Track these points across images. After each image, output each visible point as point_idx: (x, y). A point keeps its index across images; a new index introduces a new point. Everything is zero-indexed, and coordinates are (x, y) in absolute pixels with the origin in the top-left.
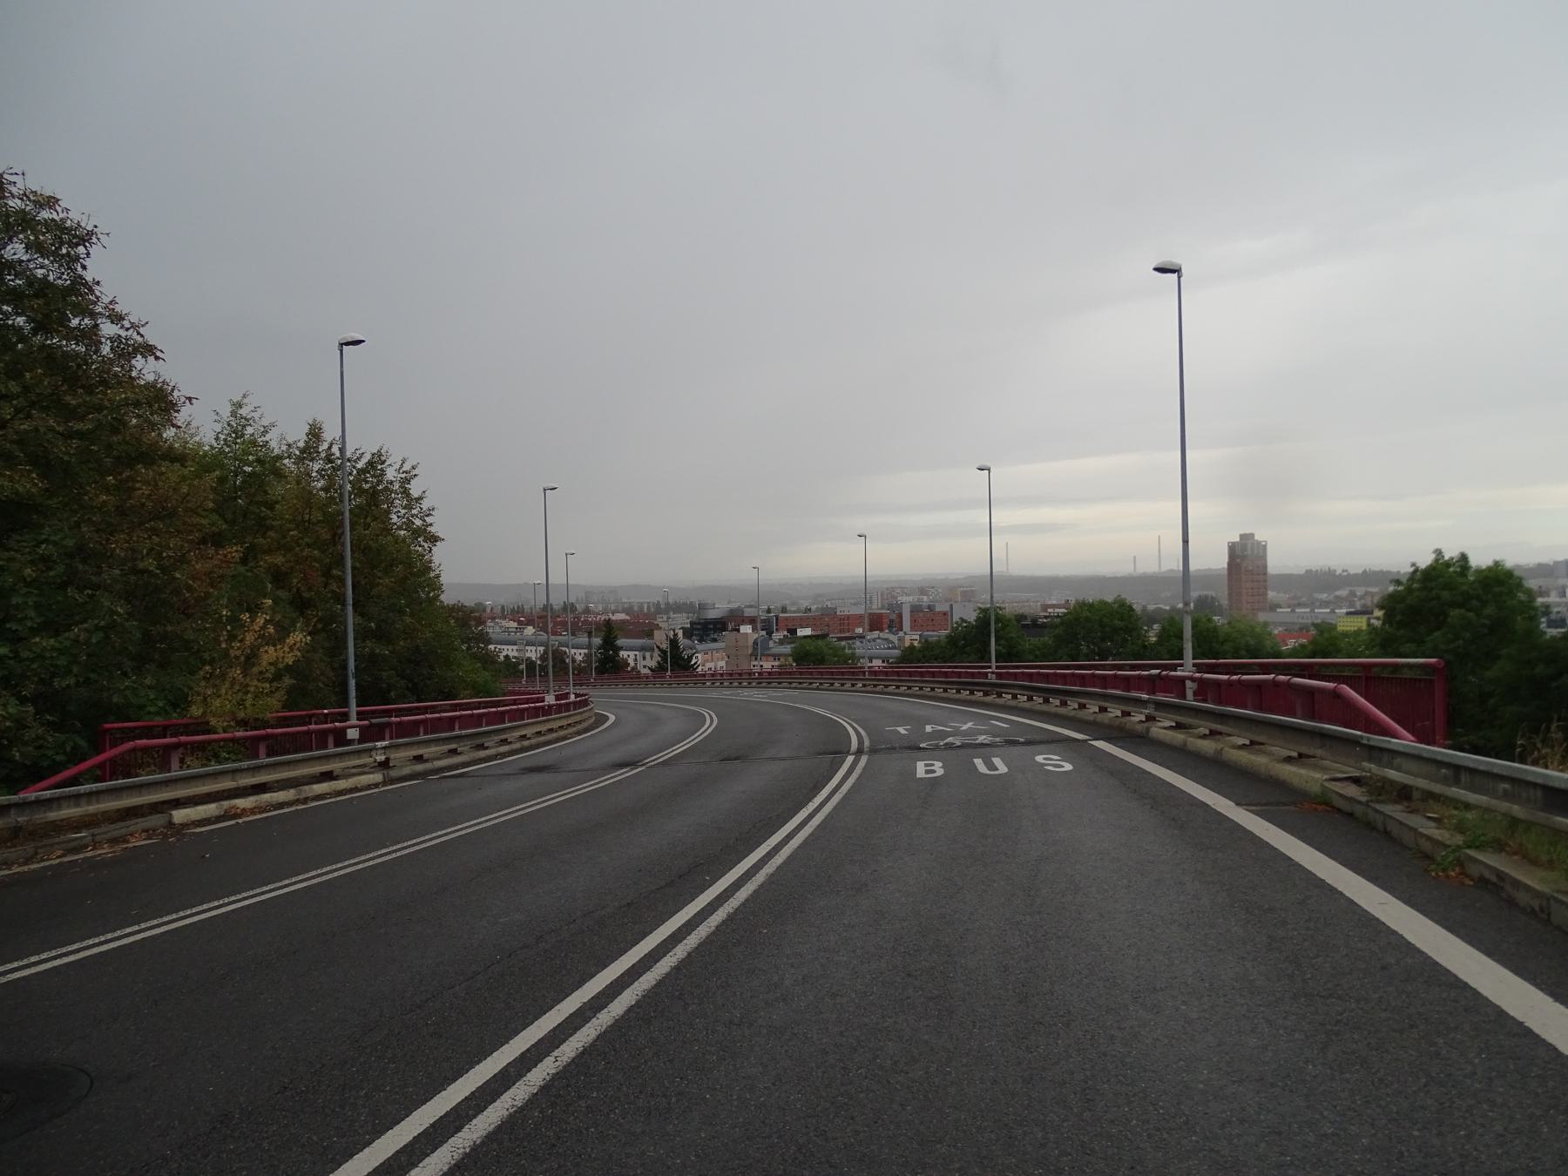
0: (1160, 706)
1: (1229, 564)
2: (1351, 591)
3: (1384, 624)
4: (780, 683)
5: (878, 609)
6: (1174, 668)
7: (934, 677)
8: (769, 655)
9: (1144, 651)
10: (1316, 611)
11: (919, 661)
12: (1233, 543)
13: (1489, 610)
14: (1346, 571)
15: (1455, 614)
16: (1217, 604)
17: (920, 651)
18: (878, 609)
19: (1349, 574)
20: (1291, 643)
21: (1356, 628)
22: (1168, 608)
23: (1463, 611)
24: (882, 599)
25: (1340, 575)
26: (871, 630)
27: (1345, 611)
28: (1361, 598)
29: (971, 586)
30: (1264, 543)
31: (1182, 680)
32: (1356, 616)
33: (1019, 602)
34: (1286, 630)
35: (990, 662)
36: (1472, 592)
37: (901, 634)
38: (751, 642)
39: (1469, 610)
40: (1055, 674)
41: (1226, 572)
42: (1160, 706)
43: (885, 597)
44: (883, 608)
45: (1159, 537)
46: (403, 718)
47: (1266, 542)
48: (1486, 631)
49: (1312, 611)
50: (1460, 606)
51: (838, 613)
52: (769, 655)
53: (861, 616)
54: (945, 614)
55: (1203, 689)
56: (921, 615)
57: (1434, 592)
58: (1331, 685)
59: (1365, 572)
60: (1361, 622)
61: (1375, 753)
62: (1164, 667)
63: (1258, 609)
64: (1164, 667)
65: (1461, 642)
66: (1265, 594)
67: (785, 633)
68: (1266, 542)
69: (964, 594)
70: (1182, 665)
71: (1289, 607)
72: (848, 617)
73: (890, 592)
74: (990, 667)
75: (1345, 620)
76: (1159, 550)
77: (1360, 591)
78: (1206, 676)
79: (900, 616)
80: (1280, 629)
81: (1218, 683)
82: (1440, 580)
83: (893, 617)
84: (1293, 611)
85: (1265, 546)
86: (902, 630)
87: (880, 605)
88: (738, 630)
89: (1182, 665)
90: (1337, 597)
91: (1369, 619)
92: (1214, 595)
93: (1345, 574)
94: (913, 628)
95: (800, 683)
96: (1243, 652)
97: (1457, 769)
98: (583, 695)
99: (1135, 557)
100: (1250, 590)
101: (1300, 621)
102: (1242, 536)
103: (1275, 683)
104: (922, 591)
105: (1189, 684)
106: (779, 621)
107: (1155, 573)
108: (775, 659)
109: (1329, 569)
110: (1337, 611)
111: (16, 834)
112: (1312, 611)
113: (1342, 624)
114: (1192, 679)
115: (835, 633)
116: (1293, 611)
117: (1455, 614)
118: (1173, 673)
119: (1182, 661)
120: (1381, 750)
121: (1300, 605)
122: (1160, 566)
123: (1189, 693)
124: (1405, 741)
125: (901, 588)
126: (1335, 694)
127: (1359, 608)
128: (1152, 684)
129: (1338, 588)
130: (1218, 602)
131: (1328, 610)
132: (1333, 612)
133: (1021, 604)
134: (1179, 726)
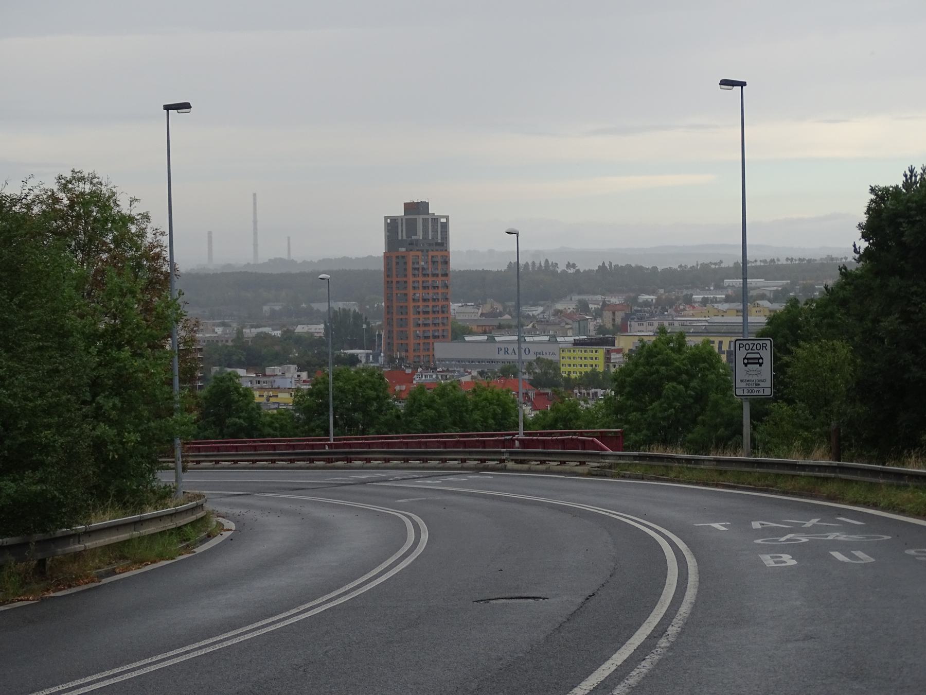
1: (387, 257)
2: (580, 301)
7: (275, 450)
13: (694, 383)
14: (574, 266)
19: (578, 271)
21: (589, 369)
22: (278, 333)
23: (675, 384)
27: (571, 339)
28: (598, 314)
30: (443, 220)
32: (588, 348)
39: (680, 383)
41: (381, 267)
45: (255, 195)
46: (506, 437)
47: (447, 218)
48: (691, 400)
58: (591, 438)
59: (602, 268)
60: (597, 358)
63: (435, 337)
66: (445, 310)
68: (447, 218)
70: (518, 434)
71: (484, 333)
75: (572, 354)
76: (255, 222)
77: (594, 301)
82: (659, 357)
84: (491, 340)
85: (445, 226)
90: (558, 312)
91: (608, 352)
93: (571, 271)
99: (210, 233)
100: (421, 304)
101: (502, 356)
109: (547, 261)
110: (559, 339)
113: (566, 361)
117: (668, 385)
120: (607, 455)
124: (610, 452)
126: (592, 441)
127: (593, 333)
128: (503, 444)
129: (560, 298)
130: (368, 324)
131: (547, 338)
132: (553, 340)
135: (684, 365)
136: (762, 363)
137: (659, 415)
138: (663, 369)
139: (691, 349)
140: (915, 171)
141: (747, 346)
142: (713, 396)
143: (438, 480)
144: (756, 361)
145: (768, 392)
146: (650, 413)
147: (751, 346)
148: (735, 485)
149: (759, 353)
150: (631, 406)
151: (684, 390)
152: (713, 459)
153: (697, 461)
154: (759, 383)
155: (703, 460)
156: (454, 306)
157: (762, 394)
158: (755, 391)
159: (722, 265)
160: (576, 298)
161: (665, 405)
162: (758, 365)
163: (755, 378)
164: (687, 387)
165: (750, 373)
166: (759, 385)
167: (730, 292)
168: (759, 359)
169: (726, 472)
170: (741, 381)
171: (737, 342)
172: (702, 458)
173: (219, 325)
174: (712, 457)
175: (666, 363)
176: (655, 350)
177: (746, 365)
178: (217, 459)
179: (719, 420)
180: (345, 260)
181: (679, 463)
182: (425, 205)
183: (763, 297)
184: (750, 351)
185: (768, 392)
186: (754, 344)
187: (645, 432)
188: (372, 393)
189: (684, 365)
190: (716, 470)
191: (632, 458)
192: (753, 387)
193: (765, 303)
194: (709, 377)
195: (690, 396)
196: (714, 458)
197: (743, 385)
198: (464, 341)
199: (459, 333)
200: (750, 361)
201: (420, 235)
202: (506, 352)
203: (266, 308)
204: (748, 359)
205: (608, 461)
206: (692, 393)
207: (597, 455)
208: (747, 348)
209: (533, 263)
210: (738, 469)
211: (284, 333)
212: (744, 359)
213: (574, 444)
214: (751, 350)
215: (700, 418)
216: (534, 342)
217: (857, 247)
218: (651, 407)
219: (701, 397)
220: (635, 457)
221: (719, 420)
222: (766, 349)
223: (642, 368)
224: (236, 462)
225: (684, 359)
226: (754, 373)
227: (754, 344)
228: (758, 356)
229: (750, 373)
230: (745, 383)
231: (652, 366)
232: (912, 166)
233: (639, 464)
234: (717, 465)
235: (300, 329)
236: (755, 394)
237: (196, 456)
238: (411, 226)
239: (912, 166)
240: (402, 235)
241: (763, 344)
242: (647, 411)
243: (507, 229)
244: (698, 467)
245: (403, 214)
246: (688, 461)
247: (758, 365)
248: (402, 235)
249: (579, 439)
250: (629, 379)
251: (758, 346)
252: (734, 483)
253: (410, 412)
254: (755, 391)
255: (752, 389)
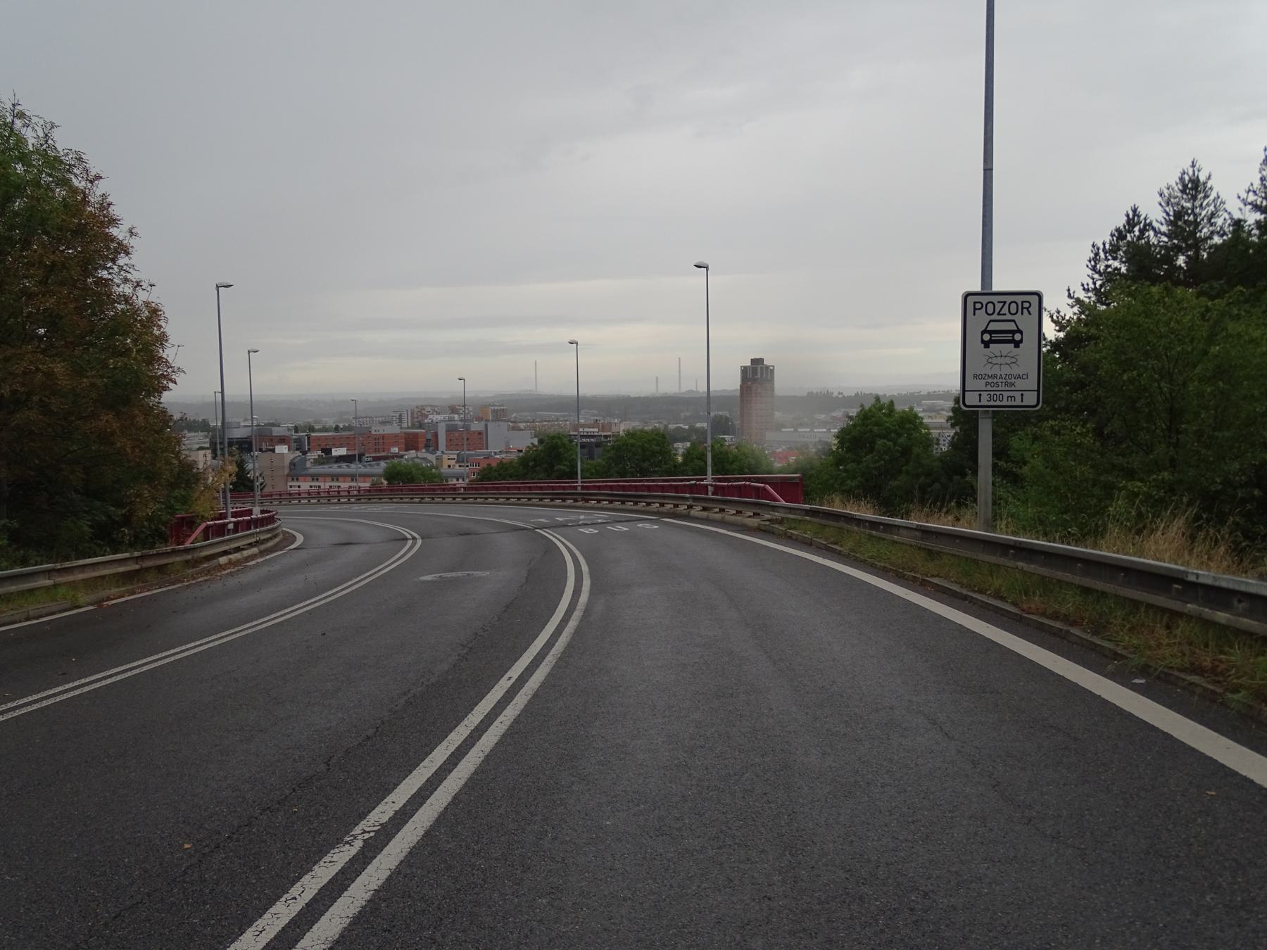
0: (695, 499)
3: (838, 448)
4: (380, 499)
5: (408, 428)
6: (702, 480)
8: (306, 475)
9: (675, 470)
10: (815, 430)
11: (496, 479)
12: (745, 367)
13: (901, 440)
14: (842, 393)
15: (880, 442)
16: (730, 423)
17: (496, 470)
18: (408, 428)
20: (777, 465)
22: (687, 427)
23: (885, 441)
24: (413, 418)
25: (837, 397)
26: (407, 449)
29: (502, 405)
30: (771, 368)
31: (706, 486)
33: (549, 421)
34: (788, 448)
35: (577, 479)
36: (892, 427)
37: (439, 453)
38: (287, 462)
39: (889, 440)
40: (618, 486)
41: (738, 394)
42: (695, 499)
43: (416, 416)
44: (413, 426)
47: (773, 366)
48: (899, 454)
49: (812, 431)
50: (884, 437)
51: (373, 433)
52: (306, 475)
53: (396, 436)
54: (480, 433)
55: (717, 490)
56: (457, 435)
57: (869, 427)
58: (763, 485)
59: (857, 394)
61: (774, 508)
62: (697, 480)
64: (697, 480)
65: (883, 462)
67: (319, 453)
68: (773, 366)
69: (495, 412)
70: (706, 479)
72: (383, 437)
73: (419, 414)
74: (577, 482)
76: (680, 372)
78: (718, 483)
79: (436, 435)
80: (784, 447)
81: (723, 486)
82: (873, 419)
83: (429, 437)
84: (796, 430)
85: (772, 371)
86: (438, 450)
87: (410, 425)
88: (273, 451)
89: (706, 479)
92: (728, 415)
93: (840, 396)
94: (449, 447)
95: (402, 498)
96: (746, 470)
97: (790, 509)
98: (269, 512)
99: (657, 378)
102: (753, 361)
103: (745, 485)
104: (453, 410)
105: (710, 488)
106: (311, 441)
107: (676, 393)
108: (313, 479)
109: (828, 391)
111: (7, 598)
112: (812, 431)
114: (712, 485)
115: (370, 453)
116: (796, 430)
117: (880, 442)
118: (702, 483)
119: (357, 456)
121: (802, 425)
122: (680, 388)
123: (710, 493)
125: (433, 406)
126: (764, 489)
128: (692, 489)
130: (732, 422)
131: (825, 430)
133: (550, 423)
134: (704, 509)
135: (893, 426)
136: (1021, 341)
137: (872, 466)
138: (875, 429)
139: (899, 413)
140: (1138, 210)
141: (990, 306)
142: (916, 450)
143: (614, 527)
144: (1009, 336)
145: (1031, 399)
146: (865, 464)
147: (998, 306)
148: (965, 592)
149: (1014, 321)
150: (849, 458)
151: (893, 446)
152: (915, 527)
153: (888, 528)
154: (1013, 380)
155: (899, 527)
156: (777, 414)
157: (1018, 402)
158: (1005, 398)
159: (921, 393)
160: (843, 410)
161: (876, 458)
162: (1012, 345)
163: (1006, 370)
164: (895, 444)
165: (994, 360)
166: (1013, 384)
167: (925, 407)
168: (1013, 332)
169: (939, 553)
170: (975, 376)
171: (969, 298)
172: (896, 524)
173: (657, 423)
174: (913, 522)
175: (878, 424)
176: (869, 414)
177: (987, 344)
178: (519, 496)
179: (920, 470)
180: (724, 391)
181: (858, 525)
182: (762, 360)
183: (943, 410)
184: (995, 317)
185: (1031, 399)
186: (1005, 303)
187: (859, 479)
188: (657, 448)
189: (893, 426)
190: (919, 548)
191: (804, 513)
192: (1000, 388)
193: (944, 413)
194: (914, 434)
195: (898, 451)
196: (918, 525)
197: (981, 384)
198: (781, 430)
199: (779, 427)
200: (996, 337)
201: (759, 376)
202: (804, 437)
203: (682, 415)
204: (991, 332)
205: (778, 515)
206: (900, 449)
207: (767, 505)
208: (990, 311)
209: (821, 392)
210: (969, 554)
211: (690, 427)
212: (983, 333)
213: (742, 491)
214: (999, 314)
215: (904, 468)
216: (817, 432)
217: (1071, 292)
218: (865, 459)
219: (906, 451)
220: (807, 512)
221: (920, 470)
222: (1030, 314)
223: (858, 428)
224: (370, 499)
225: (893, 421)
226: (999, 360)
227: (1005, 303)
228: (1012, 327)
229: (994, 360)
230: (983, 382)
231: (867, 426)
232: (1135, 205)
233: (810, 521)
234: (922, 539)
235: (698, 425)
236: (1005, 403)
237: (529, 494)
238: (754, 371)
239: (1135, 205)
240: (750, 375)
241: (1023, 302)
242: (862, 462)
243: (695, 263)
244: (888, 536)
245: (750, 364)
246: (874, 525)
247: (1012, 345)
248: (750, 375)
249: (752, 486)
250: (848, 437)
251: (1013, 306)
252: (962, 585)
253: (685, 463)
254: (1005, 398)
255: (998, 393)
